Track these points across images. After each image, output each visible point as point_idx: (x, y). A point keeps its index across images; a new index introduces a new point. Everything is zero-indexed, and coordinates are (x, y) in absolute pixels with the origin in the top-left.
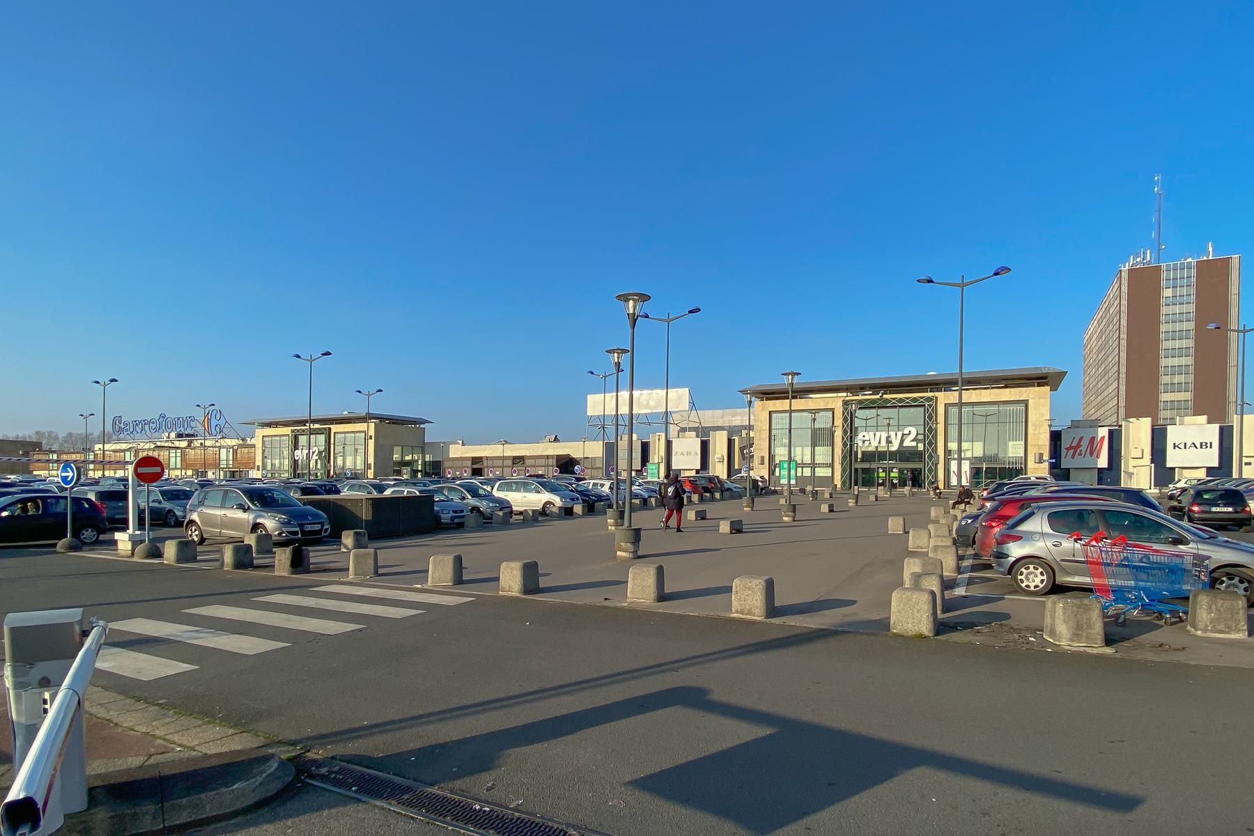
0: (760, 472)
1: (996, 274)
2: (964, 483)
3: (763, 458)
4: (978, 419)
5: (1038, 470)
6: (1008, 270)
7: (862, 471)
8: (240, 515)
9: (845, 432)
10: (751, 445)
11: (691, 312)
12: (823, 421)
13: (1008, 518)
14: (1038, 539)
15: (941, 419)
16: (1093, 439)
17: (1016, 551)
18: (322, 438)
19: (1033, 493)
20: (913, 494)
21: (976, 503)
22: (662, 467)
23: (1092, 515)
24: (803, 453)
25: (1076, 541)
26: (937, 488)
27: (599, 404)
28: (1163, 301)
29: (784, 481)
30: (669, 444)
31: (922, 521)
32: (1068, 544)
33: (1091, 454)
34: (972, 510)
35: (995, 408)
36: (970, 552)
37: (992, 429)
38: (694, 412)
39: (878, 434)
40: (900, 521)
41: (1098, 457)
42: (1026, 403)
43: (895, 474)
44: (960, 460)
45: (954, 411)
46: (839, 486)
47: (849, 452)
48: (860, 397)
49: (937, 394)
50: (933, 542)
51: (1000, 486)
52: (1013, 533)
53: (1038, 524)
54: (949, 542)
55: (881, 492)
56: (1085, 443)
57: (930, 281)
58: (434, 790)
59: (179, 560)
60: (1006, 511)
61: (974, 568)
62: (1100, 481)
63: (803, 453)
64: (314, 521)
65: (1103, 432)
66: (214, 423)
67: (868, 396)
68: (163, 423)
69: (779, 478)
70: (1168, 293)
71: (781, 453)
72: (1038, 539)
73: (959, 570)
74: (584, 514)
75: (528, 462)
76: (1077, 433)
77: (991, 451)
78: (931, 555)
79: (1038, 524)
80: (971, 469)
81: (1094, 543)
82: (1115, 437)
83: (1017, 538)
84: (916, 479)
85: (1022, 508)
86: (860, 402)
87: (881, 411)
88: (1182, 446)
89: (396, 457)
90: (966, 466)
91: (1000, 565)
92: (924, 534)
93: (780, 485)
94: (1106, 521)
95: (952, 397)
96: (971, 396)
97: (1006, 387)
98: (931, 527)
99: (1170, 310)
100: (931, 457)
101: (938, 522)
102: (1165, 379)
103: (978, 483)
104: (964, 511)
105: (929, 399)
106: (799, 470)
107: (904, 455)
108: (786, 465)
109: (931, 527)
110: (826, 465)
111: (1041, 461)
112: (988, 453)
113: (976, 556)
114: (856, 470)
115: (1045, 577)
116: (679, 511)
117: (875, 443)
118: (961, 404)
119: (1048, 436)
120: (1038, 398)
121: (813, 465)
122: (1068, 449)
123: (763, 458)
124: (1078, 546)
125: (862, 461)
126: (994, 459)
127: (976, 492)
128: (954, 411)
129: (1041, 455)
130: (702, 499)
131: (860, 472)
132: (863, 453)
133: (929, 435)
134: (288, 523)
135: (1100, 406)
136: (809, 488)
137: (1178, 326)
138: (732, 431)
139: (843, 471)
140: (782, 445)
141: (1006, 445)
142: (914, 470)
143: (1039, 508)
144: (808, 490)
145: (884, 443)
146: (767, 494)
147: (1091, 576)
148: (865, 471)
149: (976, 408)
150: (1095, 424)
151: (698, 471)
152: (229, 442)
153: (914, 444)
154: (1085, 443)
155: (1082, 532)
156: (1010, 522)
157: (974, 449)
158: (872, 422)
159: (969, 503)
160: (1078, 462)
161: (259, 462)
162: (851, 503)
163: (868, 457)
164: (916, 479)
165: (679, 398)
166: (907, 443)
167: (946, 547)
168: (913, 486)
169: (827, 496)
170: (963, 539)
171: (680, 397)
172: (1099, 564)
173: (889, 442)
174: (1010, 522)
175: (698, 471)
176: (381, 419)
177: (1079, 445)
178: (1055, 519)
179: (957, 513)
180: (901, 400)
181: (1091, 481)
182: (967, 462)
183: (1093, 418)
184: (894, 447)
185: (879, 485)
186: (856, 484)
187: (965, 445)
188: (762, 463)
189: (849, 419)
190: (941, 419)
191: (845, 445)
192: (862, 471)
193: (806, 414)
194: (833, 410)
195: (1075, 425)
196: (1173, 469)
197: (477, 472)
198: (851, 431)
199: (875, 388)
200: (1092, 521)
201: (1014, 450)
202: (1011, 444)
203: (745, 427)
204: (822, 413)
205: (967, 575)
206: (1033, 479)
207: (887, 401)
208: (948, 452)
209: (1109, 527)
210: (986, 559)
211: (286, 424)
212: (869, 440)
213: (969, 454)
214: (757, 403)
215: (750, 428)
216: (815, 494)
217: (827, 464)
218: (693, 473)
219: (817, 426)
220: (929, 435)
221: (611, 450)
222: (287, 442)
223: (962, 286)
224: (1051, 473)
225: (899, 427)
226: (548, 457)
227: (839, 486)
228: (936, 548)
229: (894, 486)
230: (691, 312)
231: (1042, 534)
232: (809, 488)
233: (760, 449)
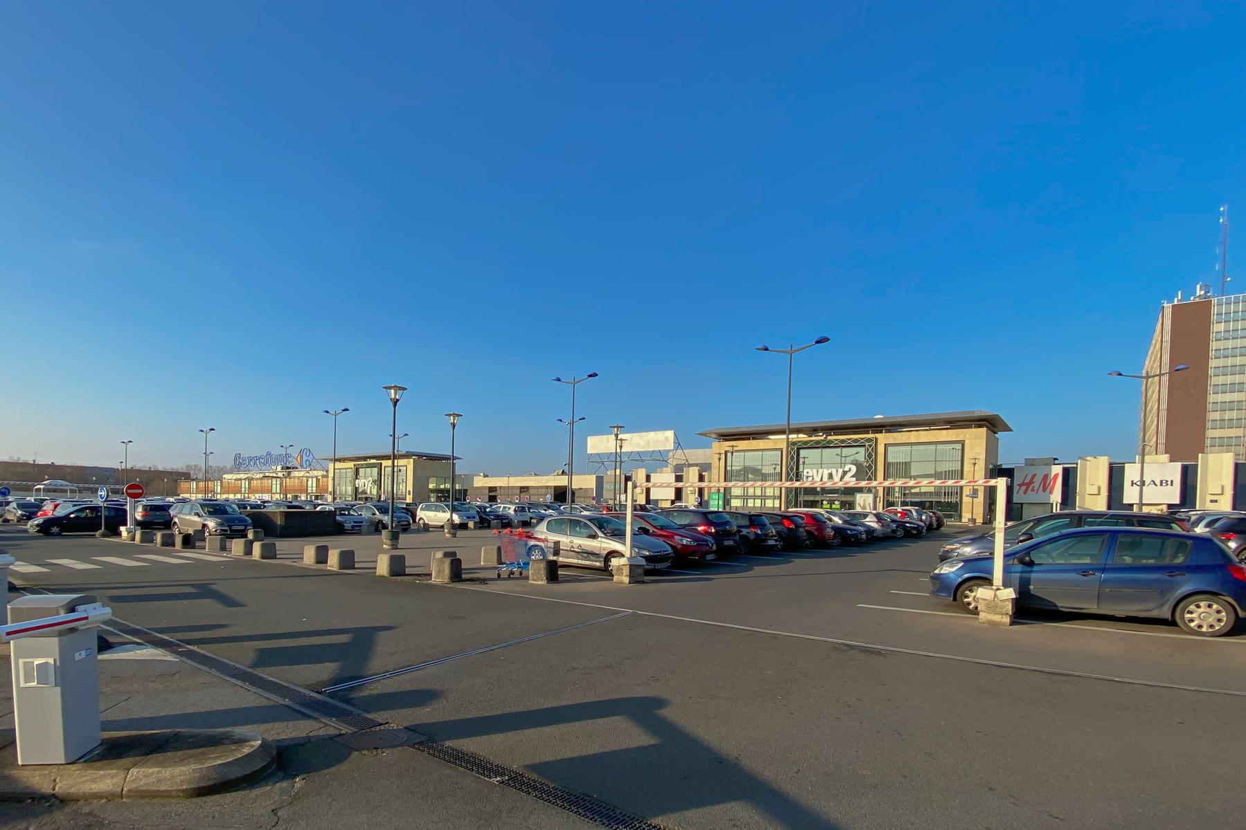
8: (196, 519)
11: (818, 342)
16: (1046, 477)
18: (375, 470)
27: (600, 444)
38: (680, 451)
41: (1051, 493)
42: (963, 443)
49: (877, 435)
56: (1038, 480)
58: (281, 701)
59: (263, 557)
64: (241, 522)
65: (1057, 470)
66: (305, 458)
68: (269, 459)
74: (475, 528)
75: (531, 491)
76: (1033, 470)
82: (1069, 477)
89: (431, 486)
99: (1221, 345)
102: (1212, 416)
105: (869, 440)
110: (774, 498)
121: (763, 497)
122: (1020, 485)
134: (221, 525)
137: (1230, 362)
149: (940, 447)
151: (673, 502)
152: (316, 473)
154: (1038, 480)
160: (1031, 497)
161: (330, 489)
165: (662, 440)
171: (667, 439)
175: (673, 502)
176: (420, 456)
177: (1031, 482)
180: (843, 441)
195: (1030, 463)
197: (493, 499)
199: (814, 431)
207: (831, 442)
211: (351, 460)
218: (1165, 508)
221: (600, 481)
222: (350, 474)
226: (547, 487)
230: (818, 342)
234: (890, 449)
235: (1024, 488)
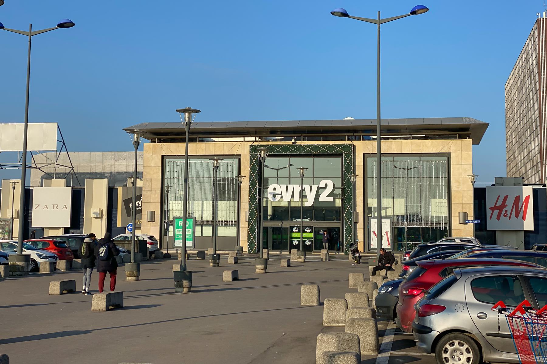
0: (149, 230)
1: (413, 13)
2: (386, 245)
3: (153, 214)
4: (398, 172)
5: (463, 231)
6: (425, 9)
7: (273, 230)
9: (252, 184)
10: (139, 198)
11: (61, 26)
12: (227, 170)
13: (428, 285)
14: (462, 310)
15: (359, 171)
16: (518, 199)
17: (439, 323)
19: (458, 257)
20: (330, 258)
21: (398, 268)
22: (17, 224)
23: (517, 284)
24: (202, 208)
25: (500, 311)
26: (356, 251)
29: (178, 243)
30: (27, 195)
31: (332, 289)
32: (494, 316)
33: (517, 215)
34: (393, 276)
35: (415, 161)
36: (392, 326)
37: (414, 184)
39: (291, 187)
40: (314, 290)
41: (524, 218)
42: (448, 156)
43: (308, 234)
44: (380, 218)
45: (372, 162)
46: (245, 249)
48: (270, 143)
49: (355, 143)
50: (349, 315)
51: (424, 249)
52: (434, 302)
53: (460, 292)
54: (367, 314)
55: (295, 256)
56: (510, 203)
57: (345, 15)
60: (428, 278)
61: (396, 346)
62: (528, 245)
63: (202, 208)
65: (527, 191)
67: (279, 142)
69: (173, 238)
71: (175, 208)
72: (462, 310)
73: (379, 348)
76: (502, 192)
77: (414, 210)
78: (347, 330)
79: (460, 292)
80: (393, 229)
81: (518, 314)
83: (441, 309)
84: (333, 240)
85: (444, 274)
86: (270, 148)
87: (294, 160)
88: (50, 207)
90: (387, 226)
91: (423, 341)
92: (340, 305)
93: (174, 247)
94: (531, 289)
96: (391, 146)
97: (426, 138)
98: (348, 296)
100: (349, 215)
101: (356, 291)
103: (400, 246)
104: (385, 278)
105: (346, 147)
106: (198, 229)
107: (319, 212)
108: (181, 223)
109: (348, 296)
111: (465, 221)
112: (411, 211)
113: (398, 331)
114: (266, 229)
115: (471, 355)
116: (113, 274)
117: (287, 198)
118: (380, 155)
119: (471, 193)
120: (460, 151)
121: (215, 224)
122: (493, 209)
123: (153, 214)
124: (503, 317)
125: (273, 218)
126: (417, 218)
127: (398, 256)
128: (372, 162)
129: (465, 215)
130: (70, 267)
131: (270, 232)
132: (274, 209)
133: (347, 190)
135: (524, 163)
136: (210, 252)
138: (114, 180)
139: (251, 230)
140: (177, 198)
141: (429, 202)
142: (331, 228)
143: (462, 274)
144: (210, 252)
145: (297, 198)
146: (157, 258)
147: (520, 352)
148: (276, 230)
149: (424, 160)
150: (519, 182)
153: (331, 199)
154: (510, 203)
155: (508, 302)
156: (432, 290)
157: (395, 206)
158: (284, 173)
159: (390, 268)
162: (259, 269)
163: (280, 213)
164: (333, 240)
166: (324, 198)
167: (365, 320)
168: (331, 248)
169: (231, 261)
170: (383, 312)
172: (528, 338)
173: (303, 196)
174: (432, 290)
175: (66, 230)
177: (504, 205)
178: (480, 287)
179: (378, 279)
180: (316, 147)
181: (516, 244)
182: (388, 221)
183: (518, 175)
184: (309, 203)
185: (293, 247)
186: (265, 247)
187: (386, 202)
188: (152, 220)
189: (258, 167)
190: (359, 171)
191: (252, 199)
192: (273, 230)
193: (207, 160)
194: (239, 157)
195: (499, 182)
196: (495, 232)
198: (259, 184)
200: (517, 288)
201: (437, 209)
202: (434, 201)
203: (131, 175)
204: (225, 160)
205: (387, 354)
206: (458, 241)
208: (367, 210)
209: (535, 295)
210: (410, 334)
212: (282, 193)
213: (390, 213)
214: (148, 146)
215: (137, 175)
216: (216, 258)
217: (233, 222)
218: (61, 233)
219: (221, 175)
220: (347, 190)
223: (379, 22)
224: (476, 236)
225: (315, 179)
227: (245, 249)
228: (353, 321)
229: (307, 249)
230: (61, 26)
231: (466, 304)
232: (210, 252)
233: (150, 203)
234: (167, 161)
235: (496, 212)
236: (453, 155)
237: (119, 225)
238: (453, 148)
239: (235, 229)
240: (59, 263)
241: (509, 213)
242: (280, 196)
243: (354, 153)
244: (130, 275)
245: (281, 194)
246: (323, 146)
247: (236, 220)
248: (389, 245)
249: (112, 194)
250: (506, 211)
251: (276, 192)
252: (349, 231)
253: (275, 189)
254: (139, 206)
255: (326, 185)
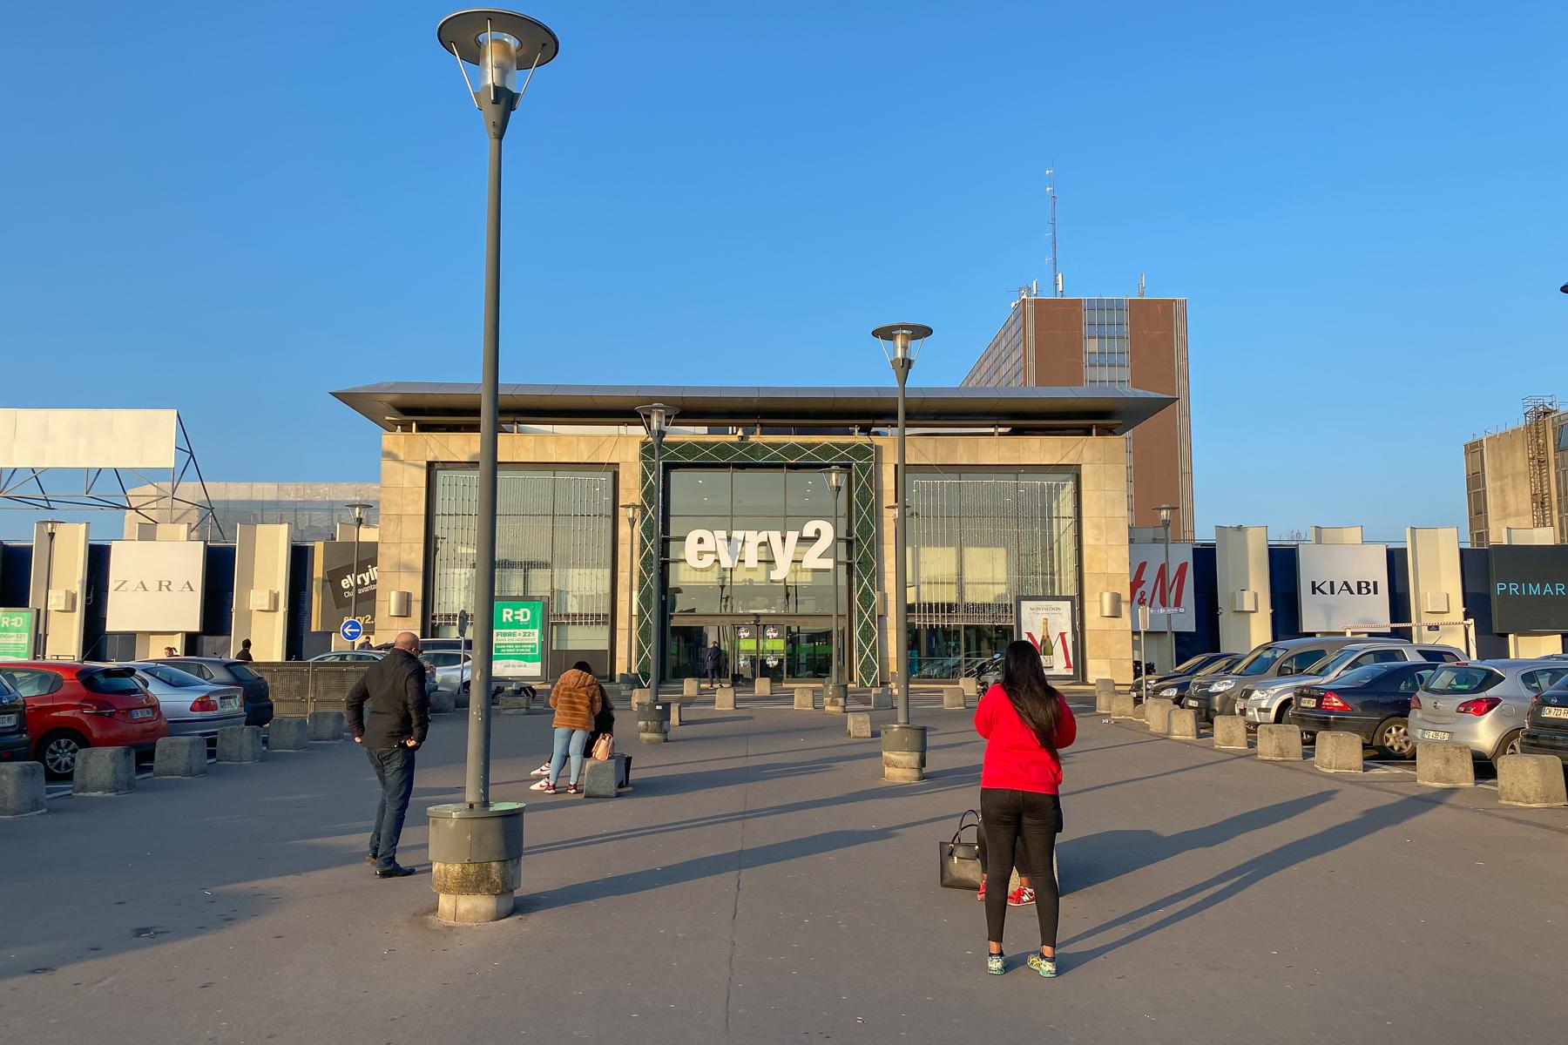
3: (406, 599)
28: (1085, 358)
30: (98, 559)
39: (738, 535)
42: (1074, 472)
47: (661, 593)
49: (877, 440)
70: (1092, 345)
88: (152, 585)
95: (927, 447)
105: (861, 451)
110: (595, 619)
165: (140, 438)
180: (793, 450)
189: (659, 502)
194: (613, 469)
200: (453, 704)
214: (394, 441)
218: (178, 643)
233: (394, 583)
234: (441, 476)
236: (1085, 471)
237: (315, 625)
238: (1087, 455)
239: (604, 632)
240: (85, 761)
241: (1148, 597)
242: (713, 557)
243: (879, 463)
244: (468, 885)
245: (715, 553)
246: (809, 446)
247: (607, 611)
248: (1068, 666)
249: (299, 558)
250: (1143, 594)
251: (702, 547)
252: (867, 634)
253: (701, 541)
254: (363, 585)
255: (818, 532)
